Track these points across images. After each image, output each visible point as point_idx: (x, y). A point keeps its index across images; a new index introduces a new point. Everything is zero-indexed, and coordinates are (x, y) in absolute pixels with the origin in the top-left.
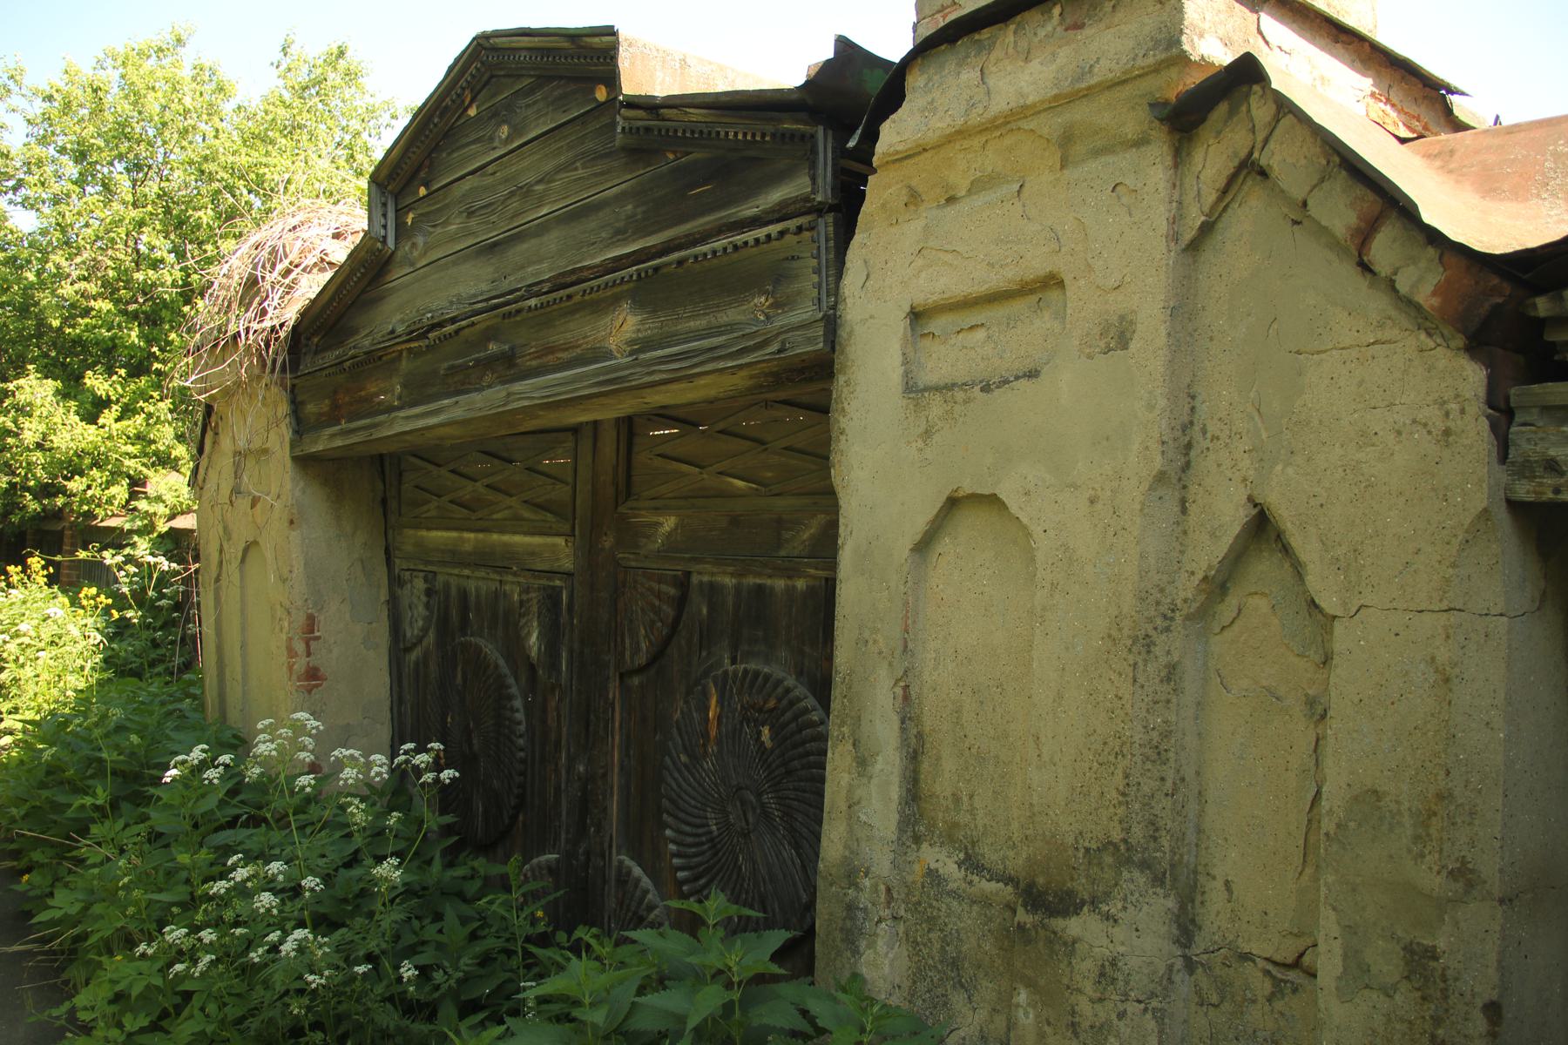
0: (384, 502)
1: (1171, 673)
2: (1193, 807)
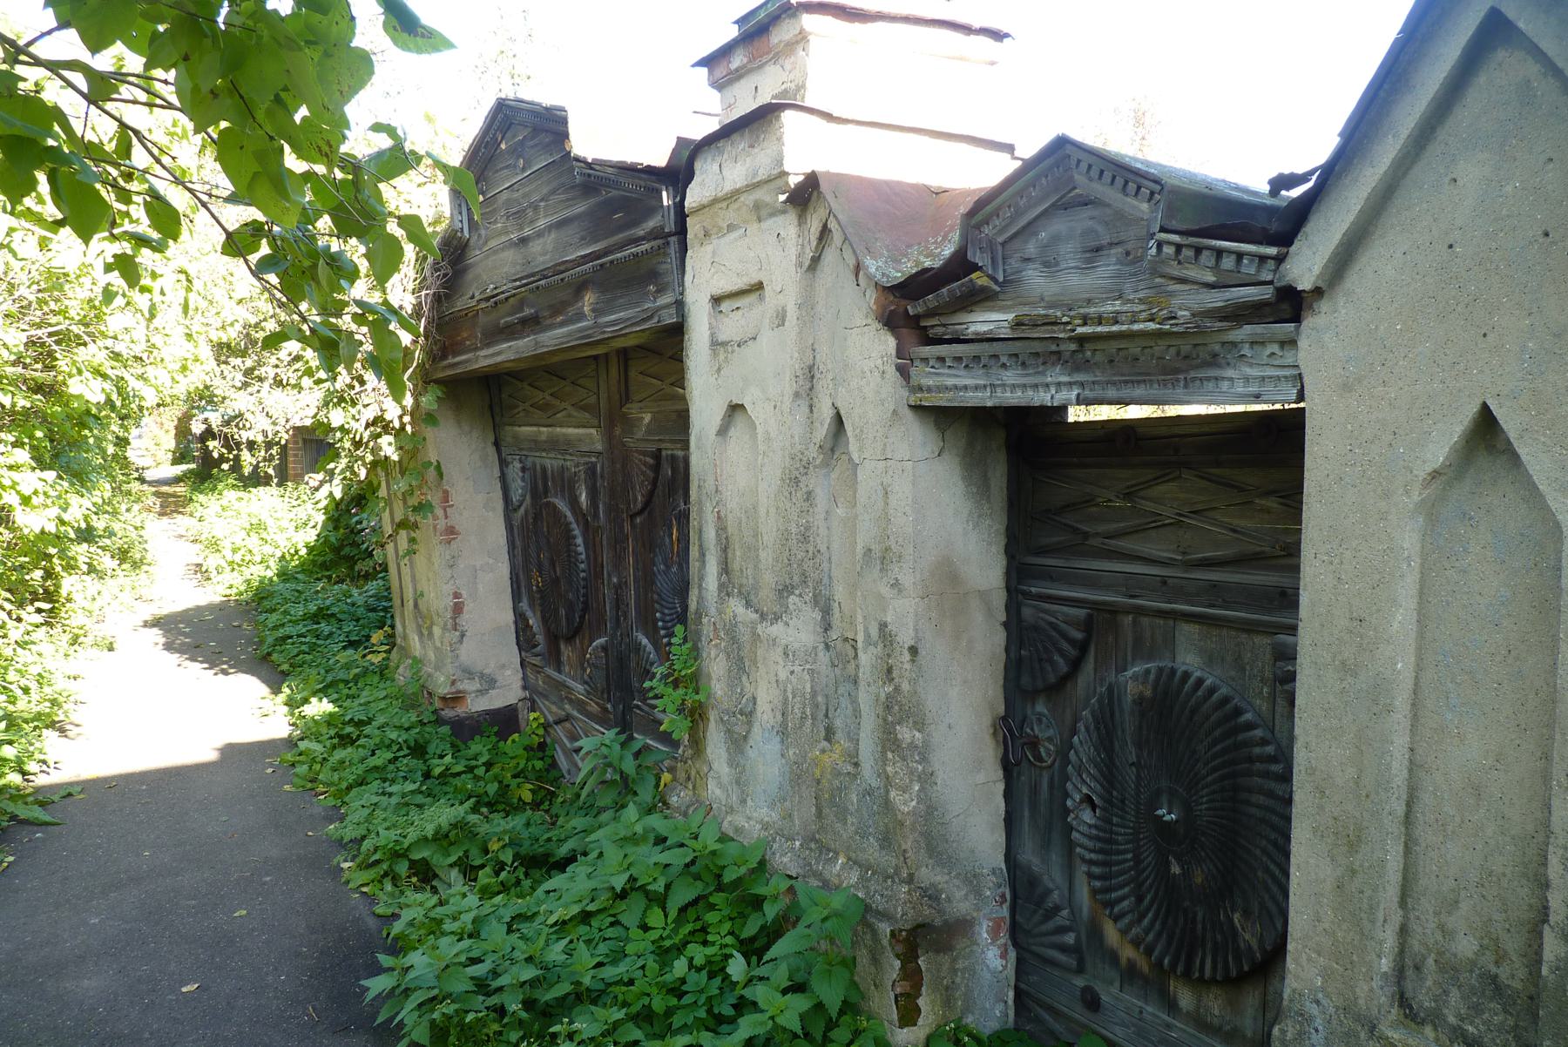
0: (491, 407)
1: (809, 496)
2: (825, 565)
